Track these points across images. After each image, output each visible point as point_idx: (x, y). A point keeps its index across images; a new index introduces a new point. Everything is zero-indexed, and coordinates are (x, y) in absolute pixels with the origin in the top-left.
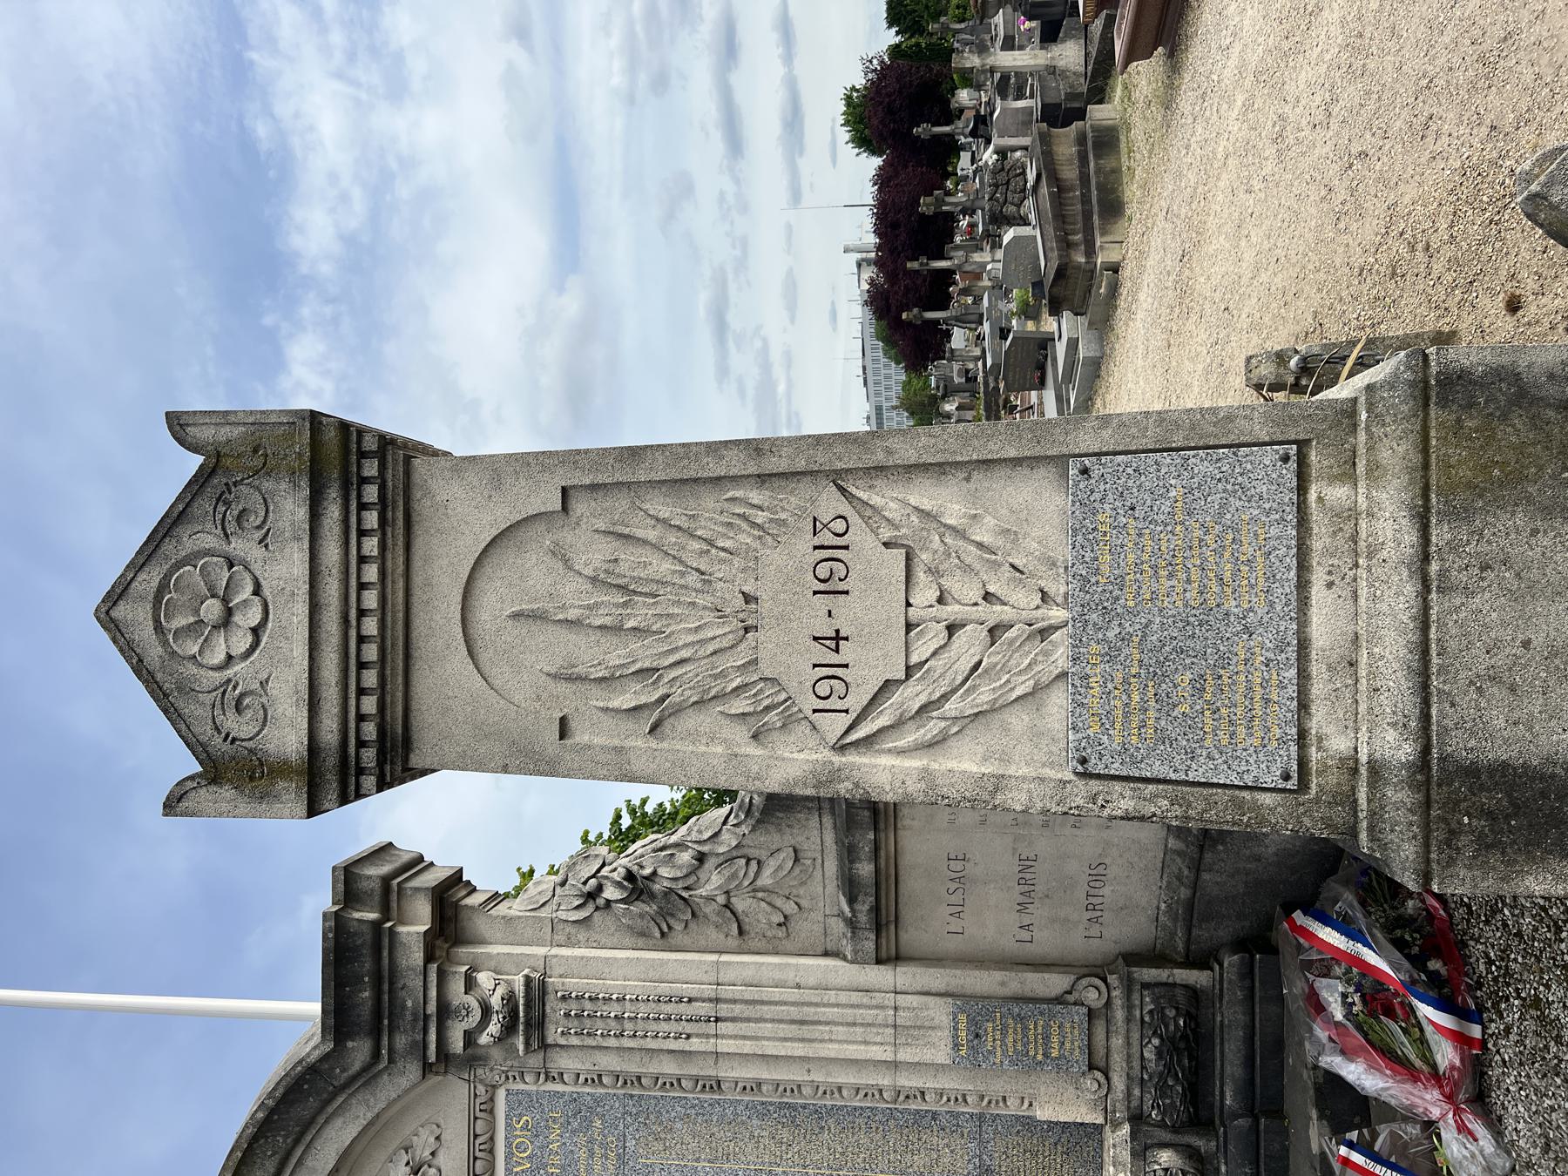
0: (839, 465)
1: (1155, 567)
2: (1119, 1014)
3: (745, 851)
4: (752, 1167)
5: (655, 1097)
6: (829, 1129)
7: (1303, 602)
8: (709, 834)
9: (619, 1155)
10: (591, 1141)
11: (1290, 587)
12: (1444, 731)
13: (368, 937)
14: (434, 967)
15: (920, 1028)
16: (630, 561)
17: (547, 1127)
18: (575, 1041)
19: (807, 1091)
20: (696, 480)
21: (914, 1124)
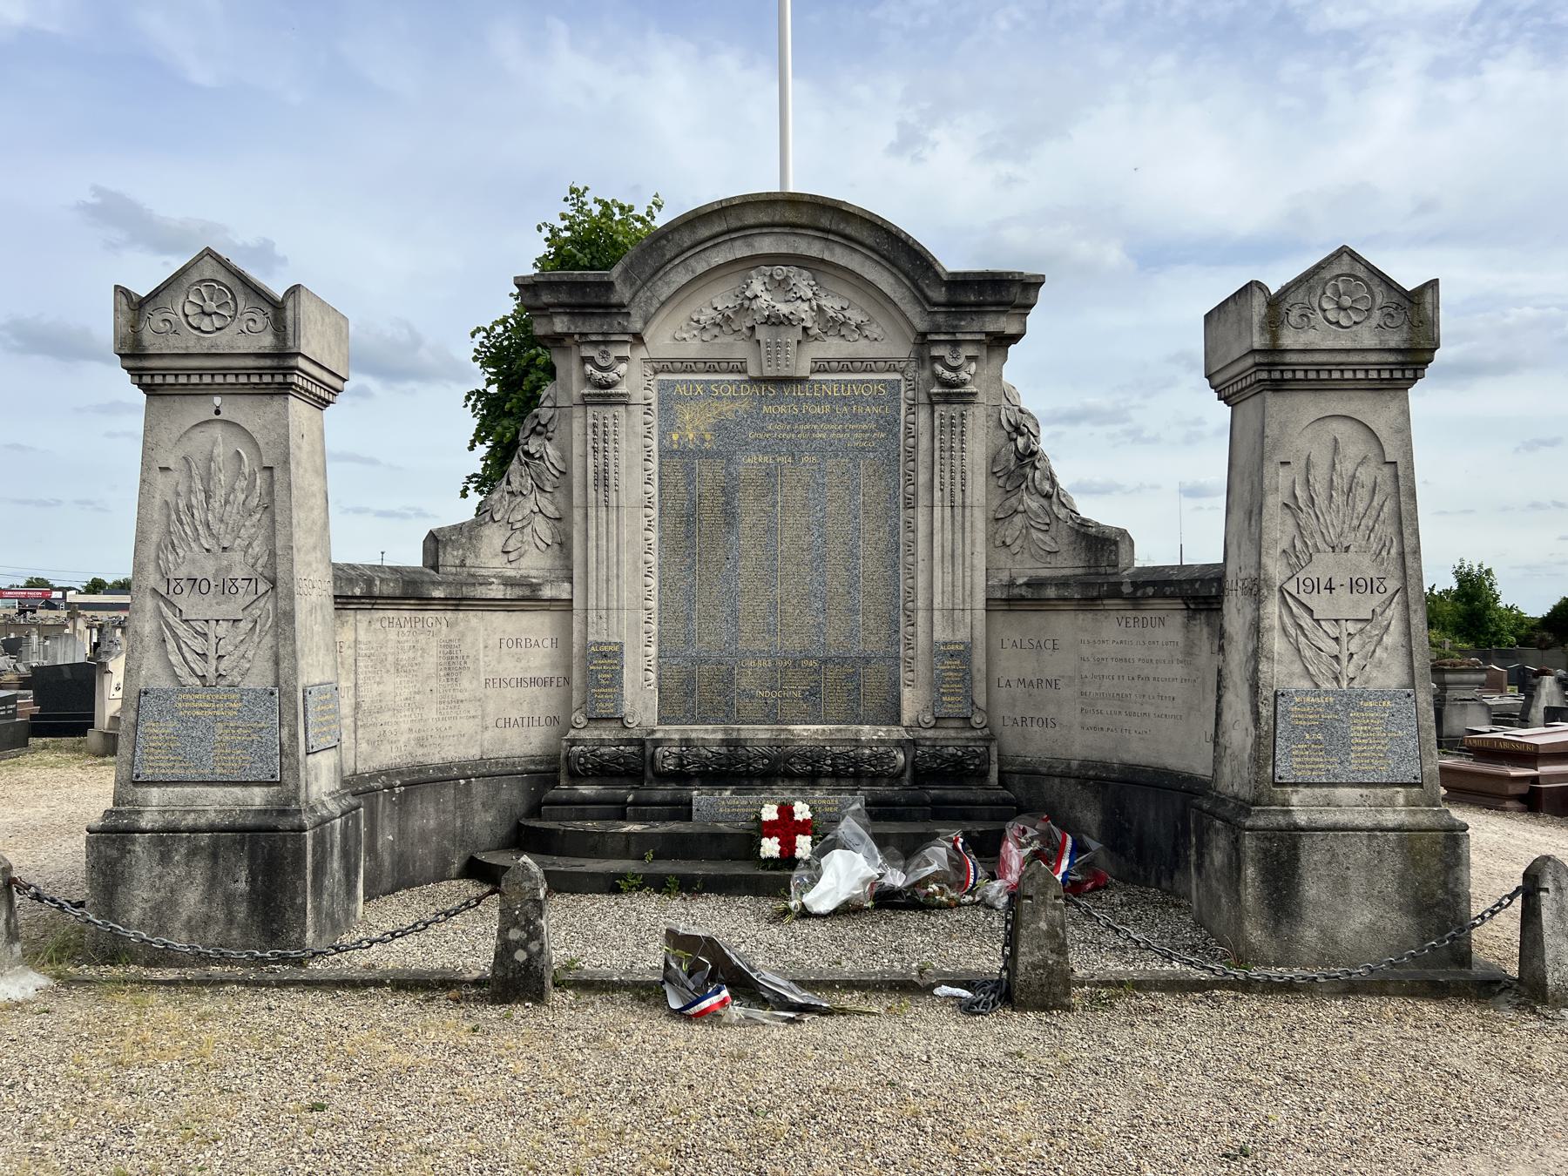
0: (1409, 590)
1: (1367, 725)
2: (968, 734)
3: (1054, 523)
7: (1352, 785)
8: (1065, 502)
10: (872, 432)
11: (1361, 779)
12: (1311, 836)
13: (1006, 299)
14: (983, 337)
15: (953, 623)
16: (1362, 494)
17: (879, 405)
18: (937, 423)
19: (910, 559)
20: (1400, 523)
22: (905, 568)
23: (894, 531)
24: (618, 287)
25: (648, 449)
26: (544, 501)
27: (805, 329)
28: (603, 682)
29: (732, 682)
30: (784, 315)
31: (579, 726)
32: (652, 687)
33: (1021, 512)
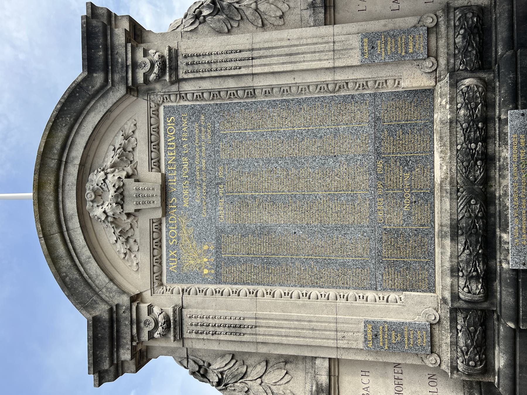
4: (270, 130)
5: (227, 104)
6: (304, 109)
9: (212, 131)
10: (200, 126)
14: (129, 45)
15: (345, 50)
17: (181, 121)
18: (191, 76)
19: (294, 89)
21: (343, 102)
22: (301, 93)
23: (273, 104)
24: (97, 313)
25: (214, 292)
26: (254, 374)
27: (128, 176)
28: (399, 338)
29: (397, 231)
30: (115, 192)
31: (439, 361)
32: (403, 297)
33: (257, 5)
